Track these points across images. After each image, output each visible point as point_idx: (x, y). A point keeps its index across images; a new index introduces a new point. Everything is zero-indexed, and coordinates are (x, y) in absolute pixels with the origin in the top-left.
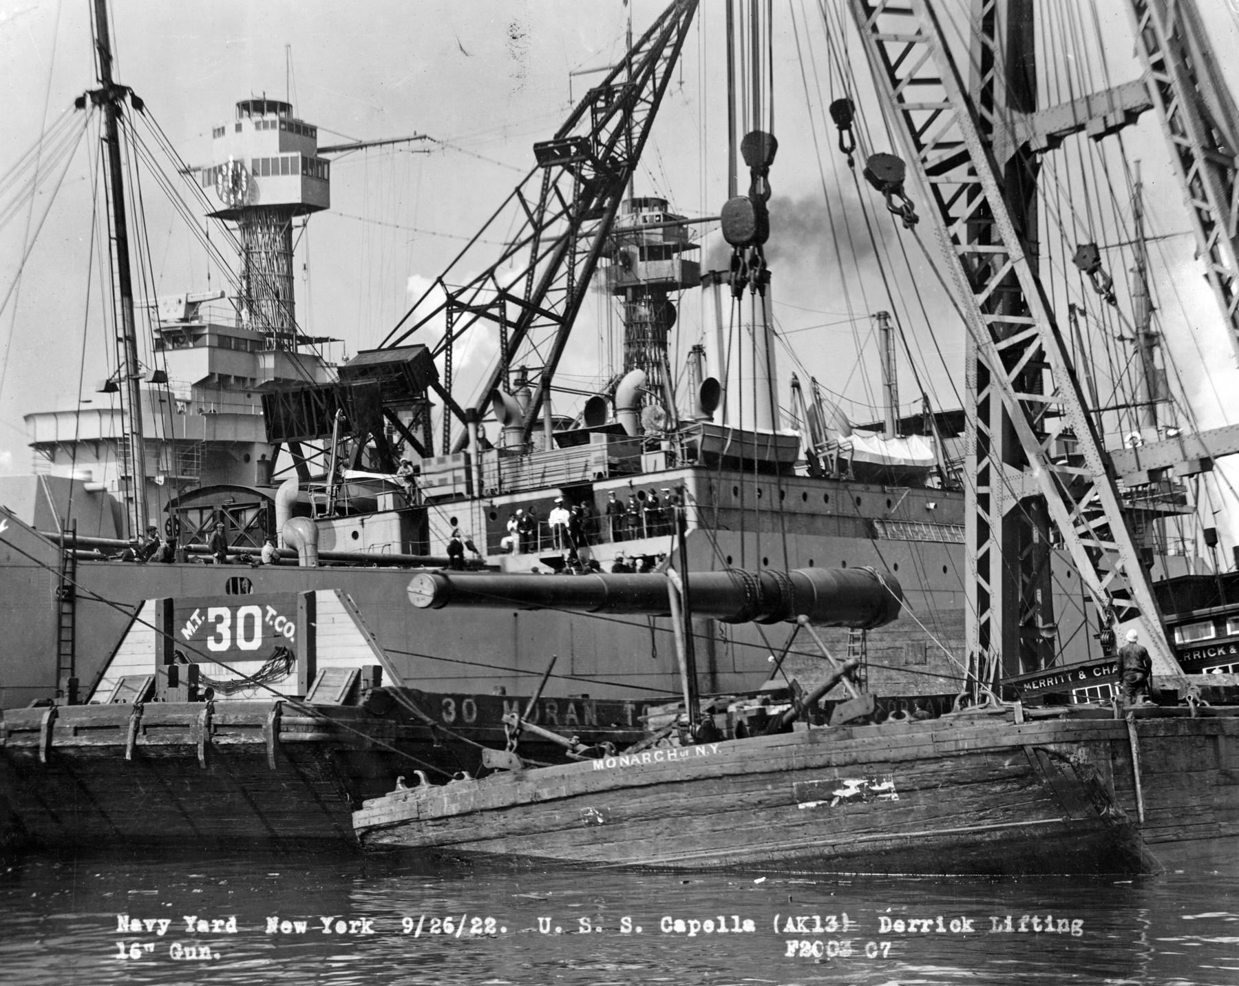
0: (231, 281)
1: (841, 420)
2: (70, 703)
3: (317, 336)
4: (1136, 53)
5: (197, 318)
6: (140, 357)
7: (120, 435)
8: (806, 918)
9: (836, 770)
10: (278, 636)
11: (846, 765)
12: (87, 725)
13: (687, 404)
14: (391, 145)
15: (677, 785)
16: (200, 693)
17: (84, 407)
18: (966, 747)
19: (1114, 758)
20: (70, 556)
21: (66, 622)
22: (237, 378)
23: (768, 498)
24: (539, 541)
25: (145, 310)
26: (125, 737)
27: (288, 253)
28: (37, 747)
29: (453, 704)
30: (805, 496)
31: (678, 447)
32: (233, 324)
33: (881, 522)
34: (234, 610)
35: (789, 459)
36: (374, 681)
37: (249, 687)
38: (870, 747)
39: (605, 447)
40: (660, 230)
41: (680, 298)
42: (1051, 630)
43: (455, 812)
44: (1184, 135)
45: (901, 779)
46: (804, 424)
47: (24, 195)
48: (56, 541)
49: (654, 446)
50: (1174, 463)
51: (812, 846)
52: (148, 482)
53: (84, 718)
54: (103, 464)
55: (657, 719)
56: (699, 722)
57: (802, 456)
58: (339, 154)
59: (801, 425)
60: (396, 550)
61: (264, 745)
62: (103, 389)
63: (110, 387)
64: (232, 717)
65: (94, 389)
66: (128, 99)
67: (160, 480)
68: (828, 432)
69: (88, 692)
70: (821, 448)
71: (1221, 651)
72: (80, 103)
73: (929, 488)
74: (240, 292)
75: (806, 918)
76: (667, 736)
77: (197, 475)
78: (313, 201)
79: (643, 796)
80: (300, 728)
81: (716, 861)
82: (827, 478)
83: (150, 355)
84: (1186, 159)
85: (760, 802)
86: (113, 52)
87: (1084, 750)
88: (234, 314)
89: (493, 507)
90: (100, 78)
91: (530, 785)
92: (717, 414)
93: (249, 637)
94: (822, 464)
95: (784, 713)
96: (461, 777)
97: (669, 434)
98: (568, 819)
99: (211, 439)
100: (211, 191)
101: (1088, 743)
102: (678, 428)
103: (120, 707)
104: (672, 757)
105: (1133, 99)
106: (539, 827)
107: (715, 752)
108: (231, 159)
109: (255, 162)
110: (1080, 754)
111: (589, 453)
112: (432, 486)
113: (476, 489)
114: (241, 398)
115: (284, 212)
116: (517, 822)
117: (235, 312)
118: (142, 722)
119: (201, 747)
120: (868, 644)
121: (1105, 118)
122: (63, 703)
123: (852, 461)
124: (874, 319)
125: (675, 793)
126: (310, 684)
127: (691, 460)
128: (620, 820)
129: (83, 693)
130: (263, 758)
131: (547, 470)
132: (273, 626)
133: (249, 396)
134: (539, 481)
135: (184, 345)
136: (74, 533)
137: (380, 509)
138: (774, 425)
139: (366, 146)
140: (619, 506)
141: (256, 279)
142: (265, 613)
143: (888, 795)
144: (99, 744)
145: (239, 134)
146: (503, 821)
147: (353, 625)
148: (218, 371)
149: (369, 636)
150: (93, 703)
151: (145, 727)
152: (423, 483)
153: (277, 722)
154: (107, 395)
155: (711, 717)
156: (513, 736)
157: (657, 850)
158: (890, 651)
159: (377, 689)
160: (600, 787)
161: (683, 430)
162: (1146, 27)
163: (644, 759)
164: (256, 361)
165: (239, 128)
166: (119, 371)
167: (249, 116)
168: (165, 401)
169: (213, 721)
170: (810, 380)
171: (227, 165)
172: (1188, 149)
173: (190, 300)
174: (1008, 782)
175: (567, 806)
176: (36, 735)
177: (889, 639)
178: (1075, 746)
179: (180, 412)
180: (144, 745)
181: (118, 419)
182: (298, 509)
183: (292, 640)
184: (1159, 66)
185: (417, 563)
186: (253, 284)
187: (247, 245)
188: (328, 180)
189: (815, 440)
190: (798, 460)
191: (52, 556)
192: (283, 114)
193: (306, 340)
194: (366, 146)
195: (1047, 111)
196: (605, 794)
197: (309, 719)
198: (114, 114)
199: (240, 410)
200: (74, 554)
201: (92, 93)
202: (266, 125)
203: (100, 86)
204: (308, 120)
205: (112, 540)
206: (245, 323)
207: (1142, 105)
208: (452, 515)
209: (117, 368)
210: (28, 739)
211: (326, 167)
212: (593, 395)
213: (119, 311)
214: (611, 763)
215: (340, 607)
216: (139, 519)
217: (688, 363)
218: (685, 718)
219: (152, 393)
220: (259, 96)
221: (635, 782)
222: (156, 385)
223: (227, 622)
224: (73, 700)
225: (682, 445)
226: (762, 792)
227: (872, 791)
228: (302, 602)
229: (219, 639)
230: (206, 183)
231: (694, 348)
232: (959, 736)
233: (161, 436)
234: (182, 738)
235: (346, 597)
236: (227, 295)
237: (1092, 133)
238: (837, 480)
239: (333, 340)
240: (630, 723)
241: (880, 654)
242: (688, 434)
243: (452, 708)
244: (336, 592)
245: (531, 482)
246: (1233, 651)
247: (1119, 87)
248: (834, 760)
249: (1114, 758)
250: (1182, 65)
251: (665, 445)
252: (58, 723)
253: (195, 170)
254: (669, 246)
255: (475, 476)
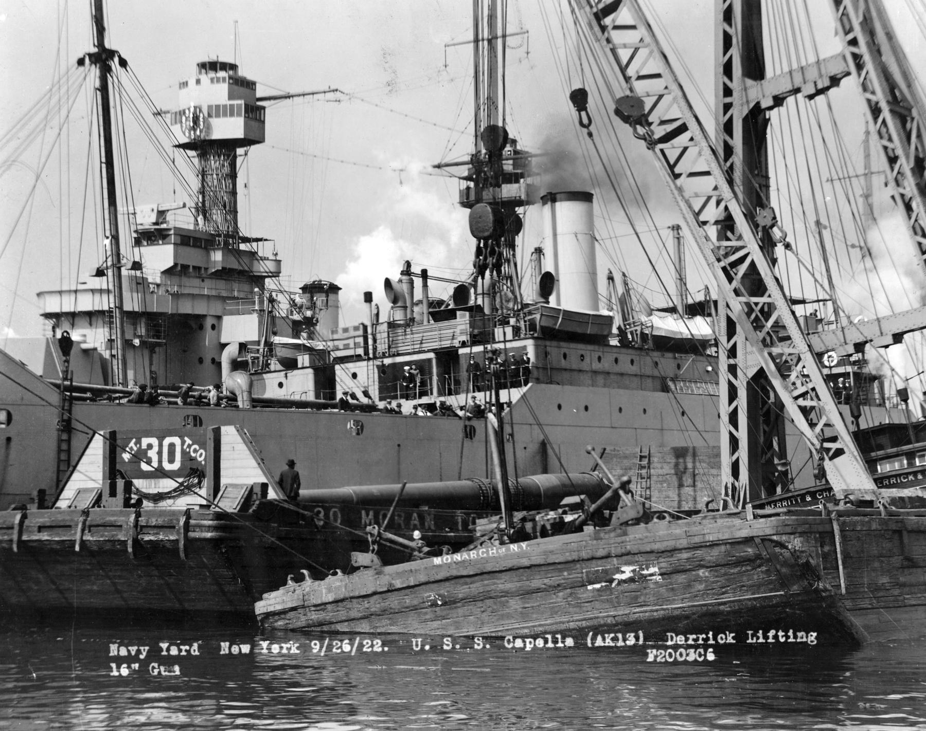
0: (190, 196)
1: (645, 305)
2: (40, 507)
3: (254, 237)
4: (836, 34)
5: (165, 222)
6: (122, 251)
7: (106, 308)
8: (612, 635)
9: (615, 559)
10: (192, 459)
11: (622, 555)
12: (48, 524)
13: (529, 292)
14: (311, 96)
15: (497, 574)
16: (133, 501)
17: (81, 287)
18: (711, 539)
19: (822, 546)
20: (67, 398)
21: (64, 446)
22: (194, 267)
23: (589, 362)
24: (417, 391)
25: (126, 216)
26: (76, 533)
27: (233, 175)
28: (11, 541)
29: (322, 513)
30: (616, 360)
31: (522, 323)
32: (191, 227)
33: (673, 380)
34: (161, 440)
35: (605, 333)
36: (261, 494)
37: (170, 498)
38: (639, 542)
39: (468, 322)
40: (511, 162)
41: (525, 214)
42: (784, 465)
43: (331, 600)
44: (873, 93)
45: (663, 565)
46: (616, 307)
47: (38, 130)
48: (57, 386)
49: (505, 322)
50: (873, 338)
51: (598, 618)
52: (127, 344)
53: (46, 519)
54: (94, 330)
55: (483, 527)
56: (514, 528)
57: (615, 331)
58: (272, 102)
59: (615, 307)
60: (311, 397)
61: (177, 541)
62: (94, 274)
63: (100, 273)
64: (154, 520)
65: (87, 274)
66: (116, 59)
67: (137, 342)
68: (634, 314)
69: (53, 500)
70: (629, 324)
71: (911, 477)
72: (81, 62)
73: (709, 355)
74: (197, 204)
75: (612, 635)
76: (490, 539)
77: (164, 339)
78: (252, 137)
79: (471, 583)
80: (204, 529)
81: (526, 631)
82: (633, 347)
83: (129, 249)
84: (876, 111)
85: (559, 585)
86: (106, 25)
87: (799, 539)
88: (192, 219)
89: (383, 365)
90: (96, 44)
91: (387, 577)
92: (552, 299)
93: (171, 460)
94: (630, 336)
95: (575, 520)
96: (335, 574)
97: (516, 314)
98: (415, 602)
99: (174, 312)
100: (176, 129)
101: (802, 534)
102: (522, 309)
103: (72, 511)
104: (493, 553)
105: (836, 69)
106: (394, 609)
107: (525, 548)
108: (192, 105)
109: (210, 107)
110: (796, 543)
111: (455, 327)
112: (338, 349)
113: (371, 352)
114: (197, 282)
115: (228, 147)
116: (378, 606)
117: (193, 218)
118: (87, 523)
119: (130, 543)
120: (652, 471)
121: (815, 83)
122: (33, 509)
123: (651, 334)
124: (670, 230)
125: (495, 581)
126: (215, 496)
127: (532, 333)
128: (455, 602)
129: (49, 499)
130: (176, 550)
131: (424, 338)
132: (189, 452)
133: (203, 281)
134: (418, 346)
135: (156, 243)
136: (71, 380)
137: (300, 365)
138: (595, 306)
139: (293, 96)
140: (476, 366)
141: (209, 193)
142: (183, 443)
143: (654, 577)
144: (56, 539)
145: (198, 87)
146: (367, 606)
147: (248, 452)
148: (180, 262)
149: (260, 461)
150: (56, 508)
151: (90, 526)
152: (331, 347)
153: (187, 524)
154: (97, 279)
155: (523, 525)
156: (374, 542)
157: (483, 623)
158: (668, 476)
159: (264, 500)
160: (439, 577)
161: (526, 310)
162: (843, 14)
163: (472, 556)
164: (208, 255)
165: (198, 82)
166: (106, 261)
167: (206, 73)
168: (141, 284)
169: (140, 523)
170: (621, 274)
171: (189, 109)
172: (877, 103)
173: (160, 209)
174: (743, 566)
175: (415, 593)
176: (10, 531)
177: (668, 468)
178: (792, 536)
179: (152, 292)
180: (89, 540)
181: (105, 297)
182: (237, 365)
183: (203, 463)
184: (854, 42)
185: (325, 406)
186: (207, 198)
187: (203, 169)
188: (264, 122)
189: (625, 319)
190: (611, 333)
191: (54, 397)
192: (231, 72)
193: (246, 240)
194: (293, 96)
195: (773, 78)
196: (443, 583)
197: (210, 522)
198: (106, 70)
199: (196, 292)
200: (71, 396)
201: (90, 55)
202: (218, 80)
203: (96, 50)
204: (250, 77)
205: (99, 387)
206: (200, 226)
207: (842, 72)
208: (353, 371)
209: (105, 259)
210: (5, 534)
211: (262, 111)
212: (460, 283)
213: (107, 216)
214: (447, 559)
215: (239, 439)
216: (120, 371)
217: (531, 260)
218: (503, 526)
219: (131, 278)
220: (213, 58)
221: (465, 573)
222: (133, 272)
223: (156, 449)
224: (42, 506)
225: (525, 321)
226: (560, 578)
227: (641, 574)
228: (210, 435)
229: (149, 462)
230: (173, 121)
231: (536, 249)
232: (705, 532)
233: (136, 309)
234: (117, 535)
235: (243, 431)
236: (188, 205)
237: (806, 94)
238: (641, 349)
239: (266, 240)
240: (460, 528)
241: (660, 479)
242: (530, 313)
243: (322, 515)
244: (235, 427)
245: (412, 347)
246: (920, 477)
247: (824, 60)
248: (613, 552)
249: (822, 546)
250: (871, 41)
251: (512, 321)
252: (27, 522)
253: (165, 113)
254: (517, 173)
255: (370, 342)
